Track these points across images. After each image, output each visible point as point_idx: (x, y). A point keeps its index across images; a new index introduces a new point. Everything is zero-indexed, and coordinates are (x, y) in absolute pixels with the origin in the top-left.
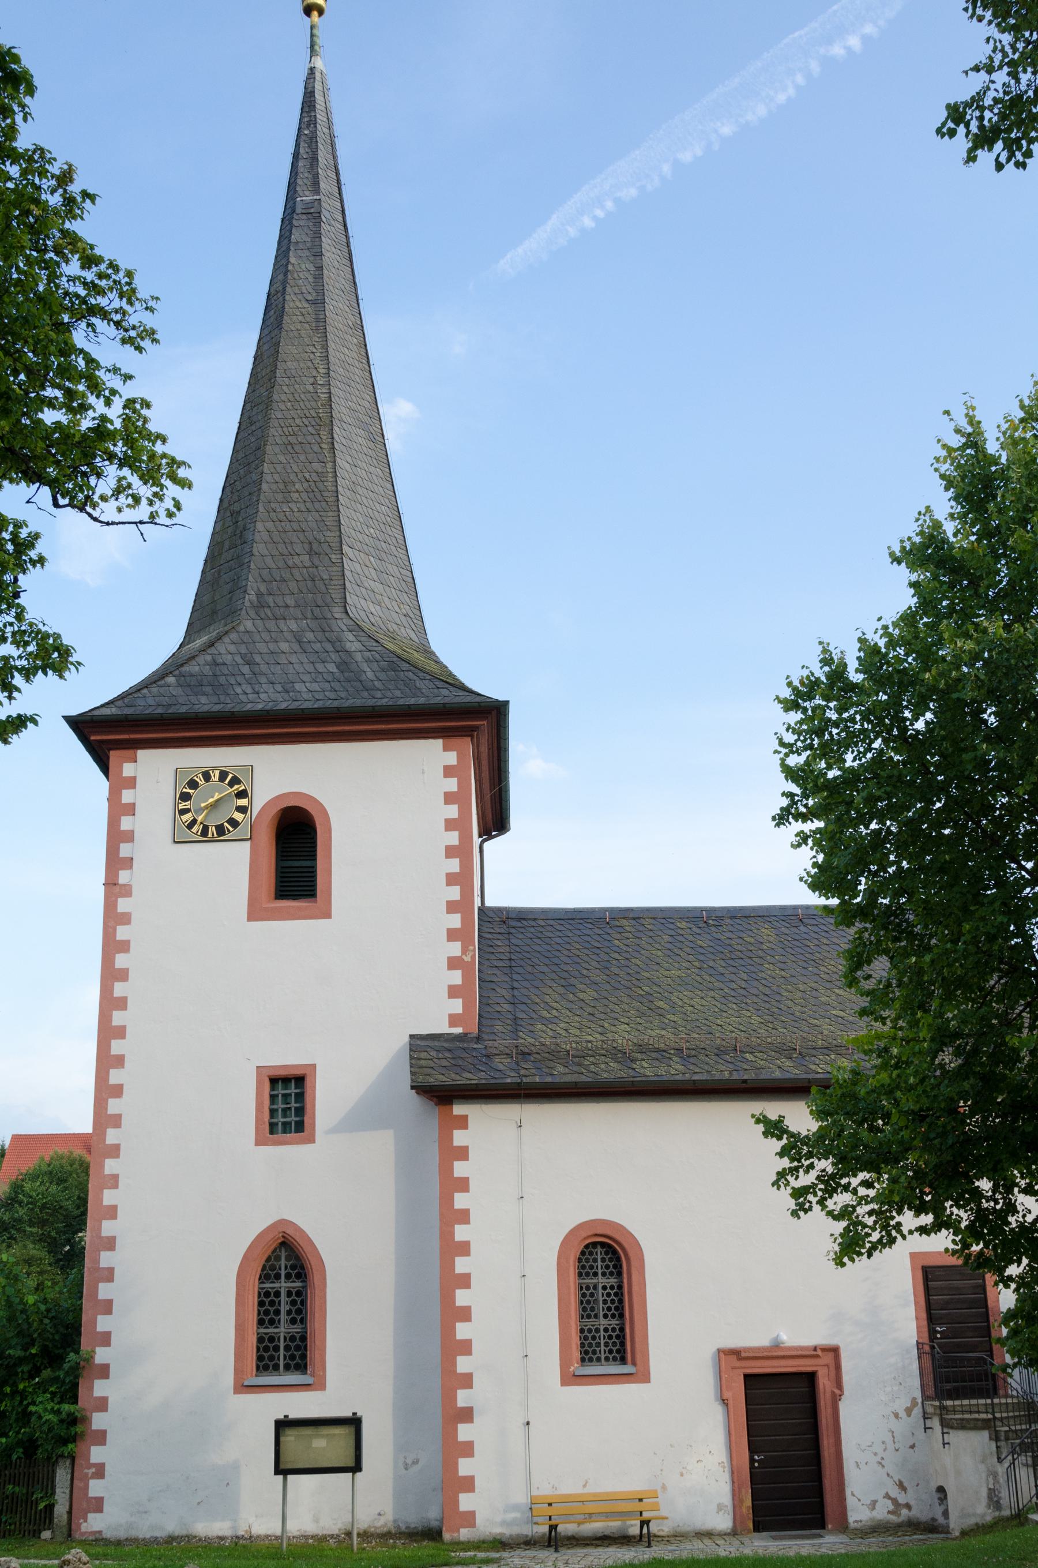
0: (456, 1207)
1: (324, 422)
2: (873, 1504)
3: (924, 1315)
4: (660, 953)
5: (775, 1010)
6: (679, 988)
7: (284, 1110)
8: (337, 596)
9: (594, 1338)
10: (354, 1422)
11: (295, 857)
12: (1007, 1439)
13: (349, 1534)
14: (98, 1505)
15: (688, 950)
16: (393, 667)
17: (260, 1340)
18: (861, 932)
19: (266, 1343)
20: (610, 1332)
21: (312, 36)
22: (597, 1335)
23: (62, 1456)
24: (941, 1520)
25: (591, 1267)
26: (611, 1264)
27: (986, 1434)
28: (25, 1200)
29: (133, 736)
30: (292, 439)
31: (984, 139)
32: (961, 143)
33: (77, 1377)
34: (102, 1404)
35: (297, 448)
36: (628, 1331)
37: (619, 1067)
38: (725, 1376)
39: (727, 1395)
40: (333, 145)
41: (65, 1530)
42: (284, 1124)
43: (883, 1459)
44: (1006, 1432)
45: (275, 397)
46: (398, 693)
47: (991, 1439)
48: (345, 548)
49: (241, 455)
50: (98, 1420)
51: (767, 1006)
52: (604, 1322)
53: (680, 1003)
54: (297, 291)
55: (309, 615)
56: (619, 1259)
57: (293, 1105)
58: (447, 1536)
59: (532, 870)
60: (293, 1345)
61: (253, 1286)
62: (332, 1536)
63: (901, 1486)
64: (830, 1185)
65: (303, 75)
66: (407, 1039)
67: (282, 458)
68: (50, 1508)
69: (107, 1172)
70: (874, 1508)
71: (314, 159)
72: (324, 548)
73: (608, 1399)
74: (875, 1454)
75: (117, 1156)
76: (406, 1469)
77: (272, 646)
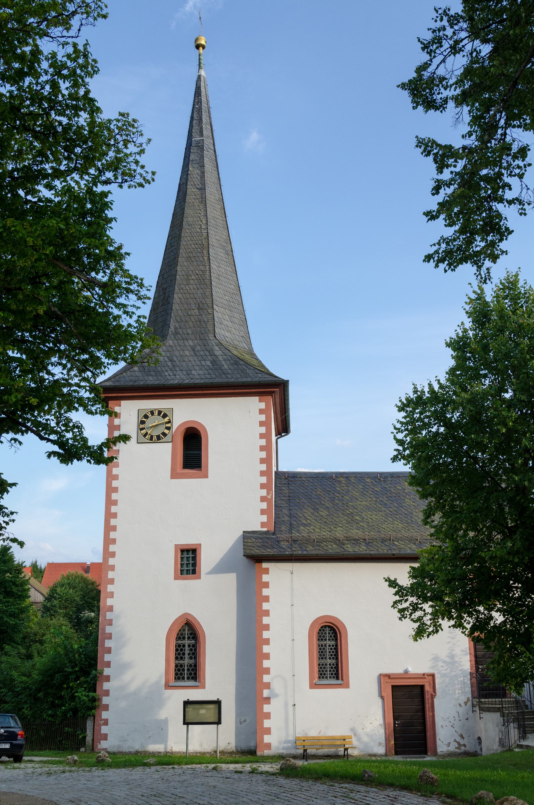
1: (204, 246)
2: (449, 744)
3: (473, 659)
5: (409, 521)
7: (187, 564)
8: (211, 329)
9: (324, 668)
10: (218, 703)
11: (192, 450)
13: (216, 752)
14: (105, 737)
15: (370, 492)
16: (236, 363)
17: (176, 666)
18: (430, 503)
19: (179, 667)
21: (200, 59)
23: (90, 715)
24: (479, 752)
25: (324, 636)
27: (499, 714)
28: (57, 596)
29: (119, 395)
30: (191, 255)
31: (441, 260)
32: (432, 263)
33: (96, 681)
34: (107, 693)
35: (193, 259)
40: (209, 112)
41: (91, 748)
42: (187, 570)
45: (183, 235)
46: (238, 376)
48: (215, 306)
49: (167, 261)
50: (105, 700)
52: (329, 661)
54: (192, 183)
55: (198, 338)
56: (336, 633)
57: (191, 562)
58: (258, 753)
59: (299, 455)
60: (191, 669)
61: (173, 643)
62: (208, 753)
63: (462, 736)
64: (415, 608)
65: (195, 79)
66: (242, 533)
67: (186, 264)
68: (84, 738)
69: (108, 590)
70: (449, 746)
71: (200, 120)
72: (205, 306)
73: (330, 695)
75: (113, 584)
77: (181, 353)
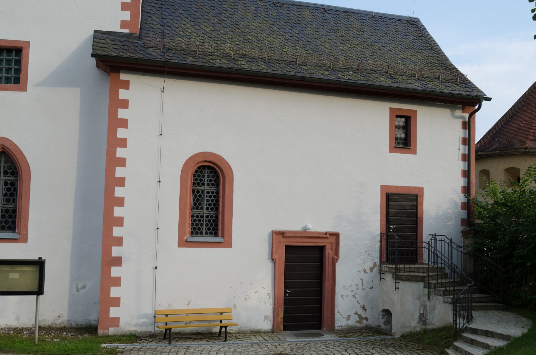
0: (118, 136)
3: (385, 219)
4: (249, 14)
6: (261, 32)
9: (199, 221)
10: (40, 264)
12: (435, 288)
20: (209, 218)
22: (202, 219)
25: (201, 180)
26: (213, 179)
27: (422, 284)
36: (220, 218)
37: (228, 62)
38: (275, 246)
39: (275, 256)
43: (356, 294)
44: (435, 283)
47: (424, 287)
51: (310, 47)
52: (206, 212)
53: (262, 39)
56: (218, 177)
58: (100, 332)
62: (27, 329)
63: (364, 308)
66: (92, 33)
70: (349, 320)
73: (206, 257)
74: (352, 291)
76: (78, 291)
